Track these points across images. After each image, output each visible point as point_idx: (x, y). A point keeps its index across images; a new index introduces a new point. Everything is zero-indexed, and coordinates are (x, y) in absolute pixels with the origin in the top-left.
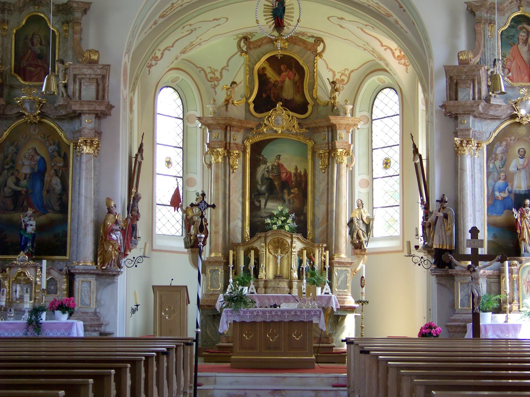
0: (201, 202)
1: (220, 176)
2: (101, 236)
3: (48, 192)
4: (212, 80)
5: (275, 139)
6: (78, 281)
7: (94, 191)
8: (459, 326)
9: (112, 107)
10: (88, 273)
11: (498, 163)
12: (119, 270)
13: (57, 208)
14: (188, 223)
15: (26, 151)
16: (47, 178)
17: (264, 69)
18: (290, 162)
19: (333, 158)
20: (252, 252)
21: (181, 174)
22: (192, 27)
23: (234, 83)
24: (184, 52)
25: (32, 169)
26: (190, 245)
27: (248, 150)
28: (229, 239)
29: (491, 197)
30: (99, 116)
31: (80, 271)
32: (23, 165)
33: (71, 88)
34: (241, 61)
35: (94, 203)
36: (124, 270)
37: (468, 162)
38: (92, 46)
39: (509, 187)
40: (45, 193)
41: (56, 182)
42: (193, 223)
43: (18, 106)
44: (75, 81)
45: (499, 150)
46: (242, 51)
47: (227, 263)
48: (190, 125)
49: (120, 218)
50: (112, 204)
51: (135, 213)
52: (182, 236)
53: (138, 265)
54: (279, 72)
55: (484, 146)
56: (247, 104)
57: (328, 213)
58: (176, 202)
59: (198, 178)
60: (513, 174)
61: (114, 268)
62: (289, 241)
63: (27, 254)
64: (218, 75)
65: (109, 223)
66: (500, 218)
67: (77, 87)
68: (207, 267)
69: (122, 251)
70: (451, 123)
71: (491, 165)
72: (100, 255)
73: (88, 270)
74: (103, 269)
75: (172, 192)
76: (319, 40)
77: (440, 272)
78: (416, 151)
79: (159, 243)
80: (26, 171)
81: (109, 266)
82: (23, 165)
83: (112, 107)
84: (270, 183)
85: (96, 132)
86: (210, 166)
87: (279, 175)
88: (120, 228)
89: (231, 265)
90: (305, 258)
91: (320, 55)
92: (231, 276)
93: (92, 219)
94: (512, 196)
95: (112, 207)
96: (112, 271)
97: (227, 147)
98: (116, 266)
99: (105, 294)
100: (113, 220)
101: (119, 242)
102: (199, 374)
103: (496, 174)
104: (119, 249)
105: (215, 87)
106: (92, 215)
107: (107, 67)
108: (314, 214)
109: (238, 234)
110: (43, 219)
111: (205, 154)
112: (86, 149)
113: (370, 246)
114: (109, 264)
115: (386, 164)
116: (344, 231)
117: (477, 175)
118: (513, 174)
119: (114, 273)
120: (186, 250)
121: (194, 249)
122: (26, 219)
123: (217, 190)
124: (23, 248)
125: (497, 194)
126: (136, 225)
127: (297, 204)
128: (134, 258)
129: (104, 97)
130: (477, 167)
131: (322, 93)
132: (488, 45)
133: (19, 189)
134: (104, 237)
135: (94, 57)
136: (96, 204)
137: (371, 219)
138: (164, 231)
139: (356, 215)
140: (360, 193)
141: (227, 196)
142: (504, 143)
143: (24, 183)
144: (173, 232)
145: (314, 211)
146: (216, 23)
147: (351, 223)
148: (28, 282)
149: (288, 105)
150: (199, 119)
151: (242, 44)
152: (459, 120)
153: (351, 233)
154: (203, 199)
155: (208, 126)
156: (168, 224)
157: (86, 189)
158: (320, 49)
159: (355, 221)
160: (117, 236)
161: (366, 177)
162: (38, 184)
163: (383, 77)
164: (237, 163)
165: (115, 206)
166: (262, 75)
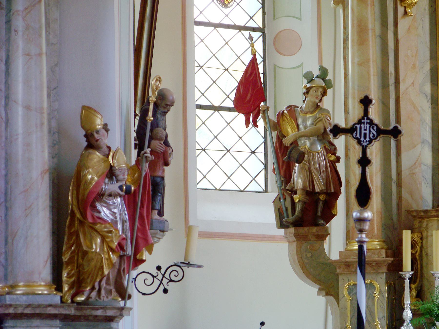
0: (360, 122)
1: (370, 26)
2: (71, 209)
7: (48, 87)
10: (40, 316)
12: (122, 304)
14: (285, 156)
21: (258, 21)
26: (291, 218)
28: (400, 198)
31: (20, 311)
35: (49, 121)
36: (136, 302)
42: (300, 159)
47: (396, 267)
50: (99, 123)
51: (157, 145)
52: (266, 191)
53: (171, 287)
58: (250, 96)
59: (306, 29)
61: (111, 299)
65: (91, 176)
68: (340, 278)
69: (129, 251)
72: (68, 263)
73: (39, 306)
74: (79, 304)
79: (205, 214)
81: (94, 294)
88: (121, 188)
89: (407, 271)
92: (407, 301)
93: (47, 167)
95: (97, 132)
96: (104, 308)
98: (114, 293)
100: (103, 168)
101: (120, 226)
104: (121, 246)
106: (46, 155)
109: (424, 186)
114: (93, 289)
119: (110, 313)
120: (282, 232)
121: (303, 230)
123: (363, 63)
126: (163, 178)
128: (159, 268)
134: (78, 215)
136: (54, 124)
138: (217, 180)
141: (392, 81)
144: (241, 180)
154: (366, 112)
156: (226, 163)
157: (27, 82)
160: (113, 212)
165: (106, 127)
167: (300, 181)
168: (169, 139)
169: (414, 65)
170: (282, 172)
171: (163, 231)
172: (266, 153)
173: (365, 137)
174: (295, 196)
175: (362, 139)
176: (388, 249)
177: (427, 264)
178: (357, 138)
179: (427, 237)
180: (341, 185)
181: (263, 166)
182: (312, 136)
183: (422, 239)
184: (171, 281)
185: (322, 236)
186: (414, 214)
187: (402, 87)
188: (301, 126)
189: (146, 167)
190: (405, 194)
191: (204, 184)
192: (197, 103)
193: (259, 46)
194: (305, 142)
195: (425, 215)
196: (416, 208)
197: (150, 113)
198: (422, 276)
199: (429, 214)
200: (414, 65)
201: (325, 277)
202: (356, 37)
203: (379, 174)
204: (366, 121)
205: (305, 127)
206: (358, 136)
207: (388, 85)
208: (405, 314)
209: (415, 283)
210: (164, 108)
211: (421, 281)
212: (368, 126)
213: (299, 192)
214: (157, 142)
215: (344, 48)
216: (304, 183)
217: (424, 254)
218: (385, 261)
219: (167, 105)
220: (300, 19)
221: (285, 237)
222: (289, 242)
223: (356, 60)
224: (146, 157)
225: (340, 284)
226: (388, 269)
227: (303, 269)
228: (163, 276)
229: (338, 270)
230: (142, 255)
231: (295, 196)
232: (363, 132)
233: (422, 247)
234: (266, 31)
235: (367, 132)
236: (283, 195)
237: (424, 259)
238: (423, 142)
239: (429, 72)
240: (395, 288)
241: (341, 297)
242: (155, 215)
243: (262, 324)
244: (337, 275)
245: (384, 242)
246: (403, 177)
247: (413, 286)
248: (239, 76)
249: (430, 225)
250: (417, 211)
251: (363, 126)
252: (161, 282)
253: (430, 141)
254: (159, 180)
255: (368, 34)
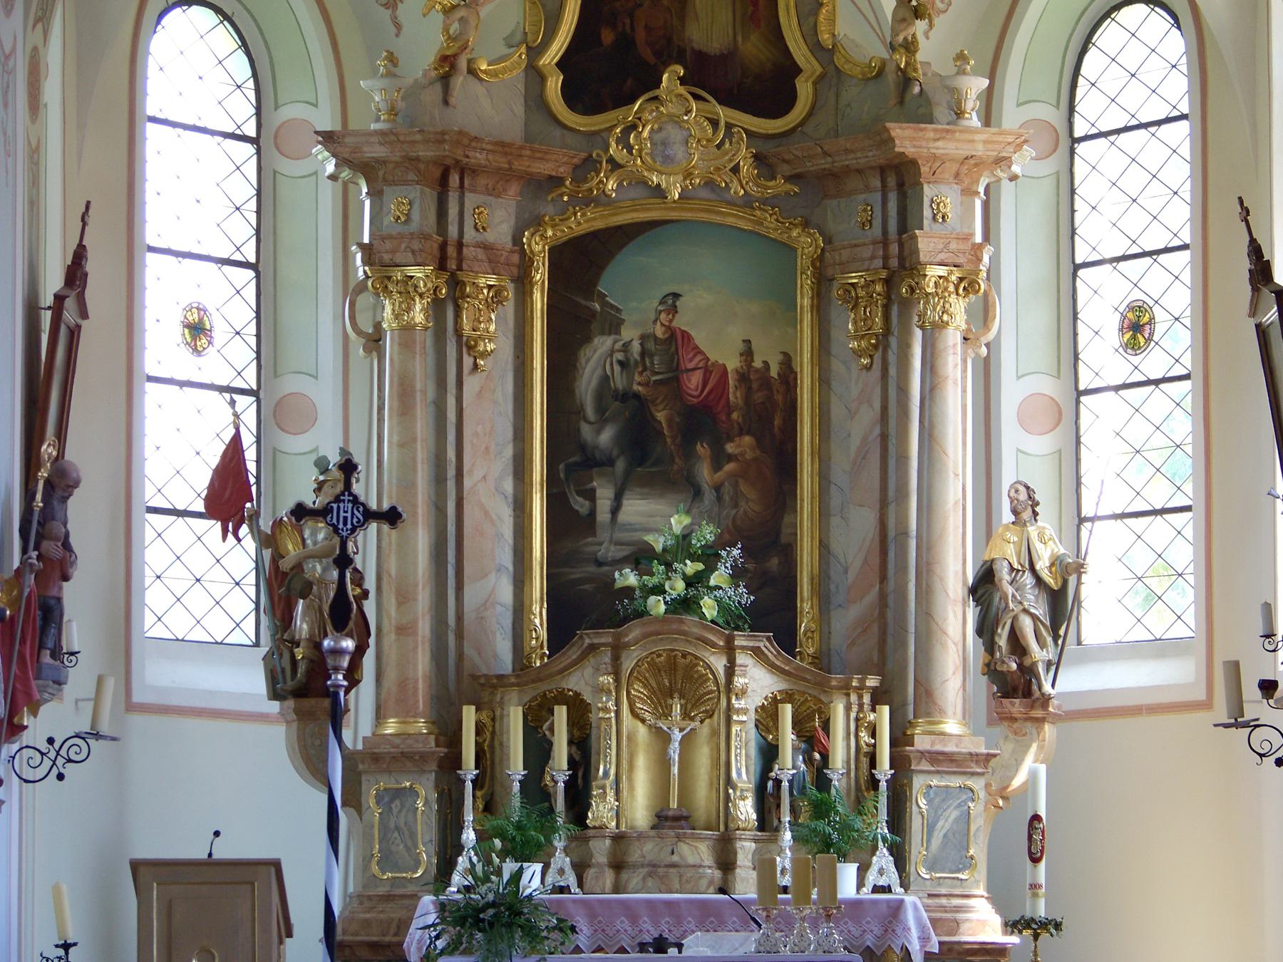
0: (337, 499)
1: (418, 386)
14: (280, 588)
28: (460, 655)
42: (305, 593)
47: (453, 761)
52: (257, 644)
53: (69, 770)
59: (324, 394)
68: (364, 778)
79: (157, 677)
89: (469, 769)
92: (469, 817)
109: (499, 638)
120: (275, 706)
121: (309, 703)
123: (406, 444)
128: (51, 741)
138: (179, 625)
141: (451, 472)
144: (219, 628)
154: (348, 485)
167: (305, 626)
168: (73, 540)
169: (487, 449)
170: (278, 613)
171: (59, 683)
172: (257, 585)
173: (345, 524)
174: (296, 650)
175: (341, 526)
176: (440, 734)
177: (501, 760)
178: (333, 525)
179: (502, 717)
180: (369, 635)
181: (253, 606)
182: (327, 556)
183: (493, 720)
184: (70, 761)
186: (482, 681)
187: (467, 483)
188: (309, 541)
189: (31, 580)
190: (468, 650)
191: (158, 631)
192: (149, 504)
193: (250, 418)
194: (314, 567)
195: (500, 681)
196: (485, 672)
197: (39, 497)
198: (493, 778)
199: (505, 680)
200: (487, 449)
202: (396, 403)
203: (428, 618)
204: (346, 498)
205: (315, 543)
206: (335, 521)
207: (446, 479)
208: (464, 836)
209: (482, 788)
210: (64, 490)
211: (492, 786)
212: (350, 505)
213: (302, 644)
214: (52, 543)
215: (379, 420)
216: (311, 629)
217: (496, 743)
218: (433, 753)
219: (69, 486)
220: (316, 378)
221: (281, 713)
222: (287, 722)
223: (396, 438)
224: (31, 565)
225: (364, 788)
226: (440, 766)
227: (306, 764)
228: (58, 753)
229: (361, 767)
230: (22, 718)
231: (296, 650)
232: (342, 514)
233: (493, 733)
234: (262, 395)
235: (349, 515)
236: (278, 648)
237: (498, 751)
238: (499, 569)
239: (511, 461)
240: (450, 795)
241: (365, 806)
242: (46, 658)
243: (217, 834)
244: (360, 774)
245: (434, 723)
246: (466, 623)
247: (479, 794)
248: (215, 461)
249: (506, 698)
250: (485, 676)
251: (342, 505)
252: (54, 763)
253: (511, 568)
254: (52, 602)
255: (415, 399)
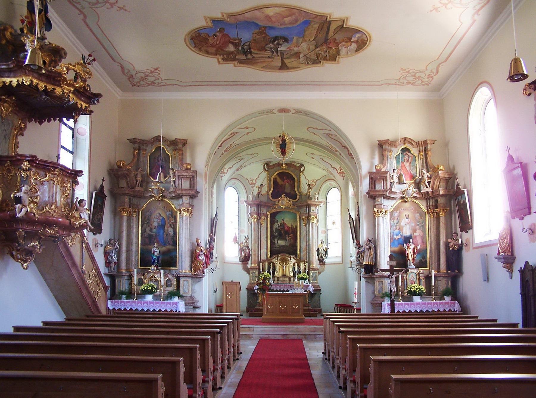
2: (194, 258)
3: (167, 235)
4: (252, 184)
5: (280, 212)
6: (182, 280)
8: (377, 303)
9: (199, 192)
11: (395, 221)
13: (171, 243)
15: (155, 215)
16: (166, 228)
17: (276, 178)
18: (288, 221)
19: (309, 220)
20: (271, 264)
22: (241, 157)
23: (262, 185)
24: (238, 170)
25: (159, 224)
27: (269, 216)
29: (392, 238)
30: (193, 197)
32: (154, 221)
33: (177, 182)
34: (265, 174)
37: (381, 219)
38: (188, 161)
39: (401, 233)
40: (165, 236)
41: (171, 230)
43: (150, 192)
44: (179, 179)
45: (396, 215)
46: (266, 170)
48: (241, 205)
49: (203, 249)
54: (283, 180)
55: (388, 214)
56: (268, 195)
57: (307, 245)
59: (246, 229)
60: (403, 227)
62: (289, 259)
63: (155, 266)
64: (254, 182)
66: (396, 249)
67: (180, 182)
69: (205, 265)
70: (371, 201)
71: (392, 222)
75: (234, 235)
76: (302, 165)
77: (367, 276)
78: (350, 216)
80: (155, 224)
82: (154, 221)
83: (199, 192)
84: (279, 232)
85: (190, 205)
86: (251, 223)
87: (284, 228)
90: (296, 267)
91: (302, 172)
94: (403, 238)
97: (259, 215)
99: (197, 287)
102: (241, 333)
103: (395, 227)
105: (253, 187)
107: (195, 172)
108: (300, 246)
110: (164, 249)
111: (249, 218)
112: (185, 214)
113: (327, 261)
115: (334, 223)
116: (315, 254)
117: (385, 227)
118: (403, 227)
122: (155, 248)
123: (255, 235)
124: (153, 263)
125: (395, 237)
127: (292, 241)
129: (194, 187)
130: (385, 223)
131: (304, 188)
132: (390, 162)
133: (152, 233)
135: (189, 167)
137: (327, 249)
139: (320, 247)
140: (322, 236)
142: (398, 211)
143: (154, 230)
145: (301, 245)
146: (253, 156)
147: (318, 250)
148: (156, 280)
149: (288, 195)
150: (245, 201)
151: (265, 167)
152: (376, 199)
153: (318, 255)
155: (250, 205)
158: (302, 169)
159: (320, 249)
160: (202, 258)
161: (324, 229)
162: (162, 231)
163: (333, 183)
164: (264, 222)
166: (275, 181)
185: (247, 264)
201: (248, 270)
